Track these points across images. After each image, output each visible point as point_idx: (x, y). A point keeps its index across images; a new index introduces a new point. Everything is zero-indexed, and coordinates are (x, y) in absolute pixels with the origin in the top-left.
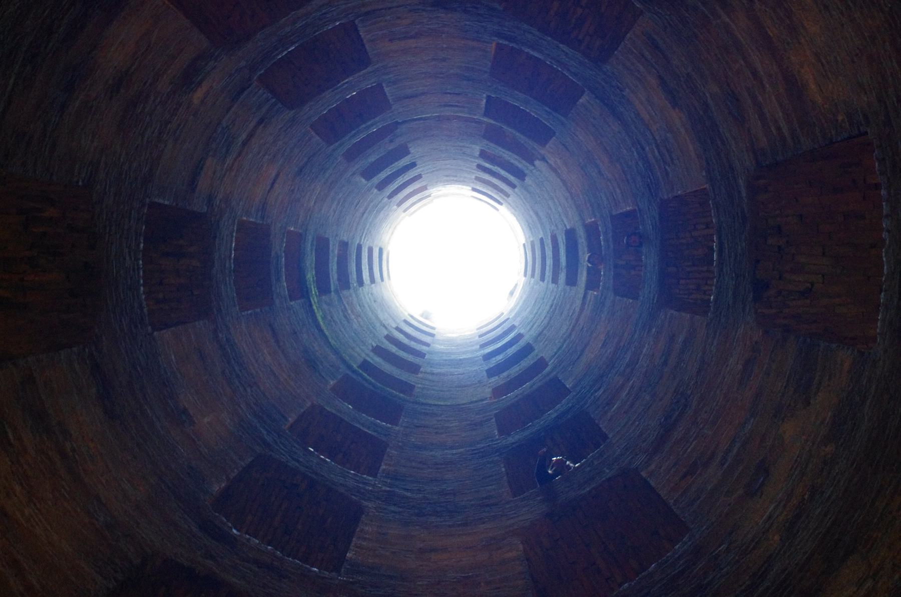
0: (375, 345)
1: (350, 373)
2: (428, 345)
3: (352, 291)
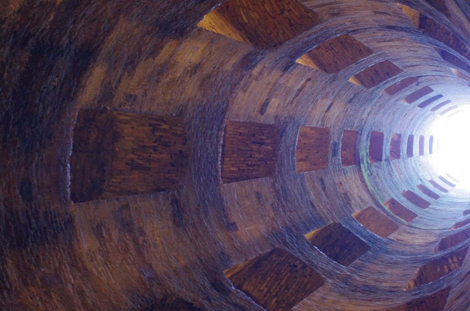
0: (406, 190)
1: (374, 206)
2: (446, 191)
3: (401, 160)
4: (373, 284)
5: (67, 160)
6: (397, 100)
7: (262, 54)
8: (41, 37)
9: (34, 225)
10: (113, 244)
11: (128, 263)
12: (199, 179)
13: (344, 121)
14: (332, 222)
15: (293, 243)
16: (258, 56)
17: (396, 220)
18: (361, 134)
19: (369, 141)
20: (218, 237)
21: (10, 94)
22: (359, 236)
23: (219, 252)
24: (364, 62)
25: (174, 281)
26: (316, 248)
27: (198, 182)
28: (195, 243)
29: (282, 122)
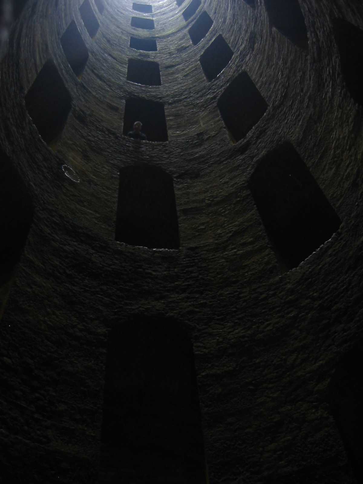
4: (249, 34)
5: (151, 251)
6: (108, 4)
7: (75, 106)
8: (65, 264)
9: (196, 275)
10: (211, 221)
11: (224, 212)
12: (165, 158)
13: (123, 47)
14: (199, 62)
15: (214, 93)
16: (77, 109)
17: (199, 12)
18: (133, 35)
19: (138, 29)
20: (208, 147)
21: (105, 288)
22: (211, 42)
23: (219, 147)
24: (80, 28)
25: (238, 181)
26: (218, 75)
27: (167, 159)
28: (212, 163)
29: (124, 94)
